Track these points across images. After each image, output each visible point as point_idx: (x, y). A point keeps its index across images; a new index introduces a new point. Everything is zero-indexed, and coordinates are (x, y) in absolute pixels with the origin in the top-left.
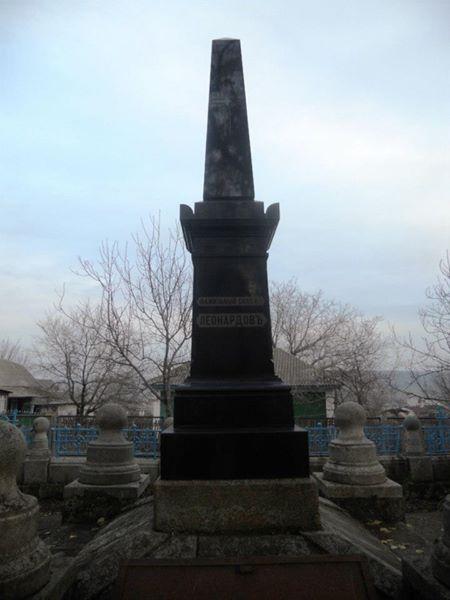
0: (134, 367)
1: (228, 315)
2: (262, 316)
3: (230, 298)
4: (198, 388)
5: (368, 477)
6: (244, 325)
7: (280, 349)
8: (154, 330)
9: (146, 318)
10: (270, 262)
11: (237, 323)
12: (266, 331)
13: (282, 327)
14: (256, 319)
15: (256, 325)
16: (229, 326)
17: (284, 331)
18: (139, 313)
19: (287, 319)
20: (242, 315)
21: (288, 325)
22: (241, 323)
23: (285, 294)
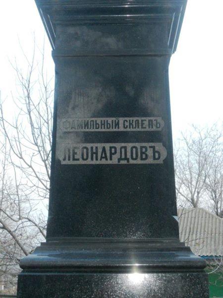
0: (10, 232)
1: (108, 146)
2: (159, 146)
3: (110, 120)
4: (60, 261)
5: (146, 257)
6: (132, 162)
7: (202, 209)
8: (35, 181)
9: (25, 166)
10: (171, 57)
11: (119, 160)
12: (166, 170)
13: (204, 181)
14: (150, 152)
15: (150, 161)
16: (109, 162)
17: (207, 186)
18: (17, 161)
19: (211, 171)
20: (129, 146)
21: (212, 178)
22: (126, 159)
23: (209, 140)
